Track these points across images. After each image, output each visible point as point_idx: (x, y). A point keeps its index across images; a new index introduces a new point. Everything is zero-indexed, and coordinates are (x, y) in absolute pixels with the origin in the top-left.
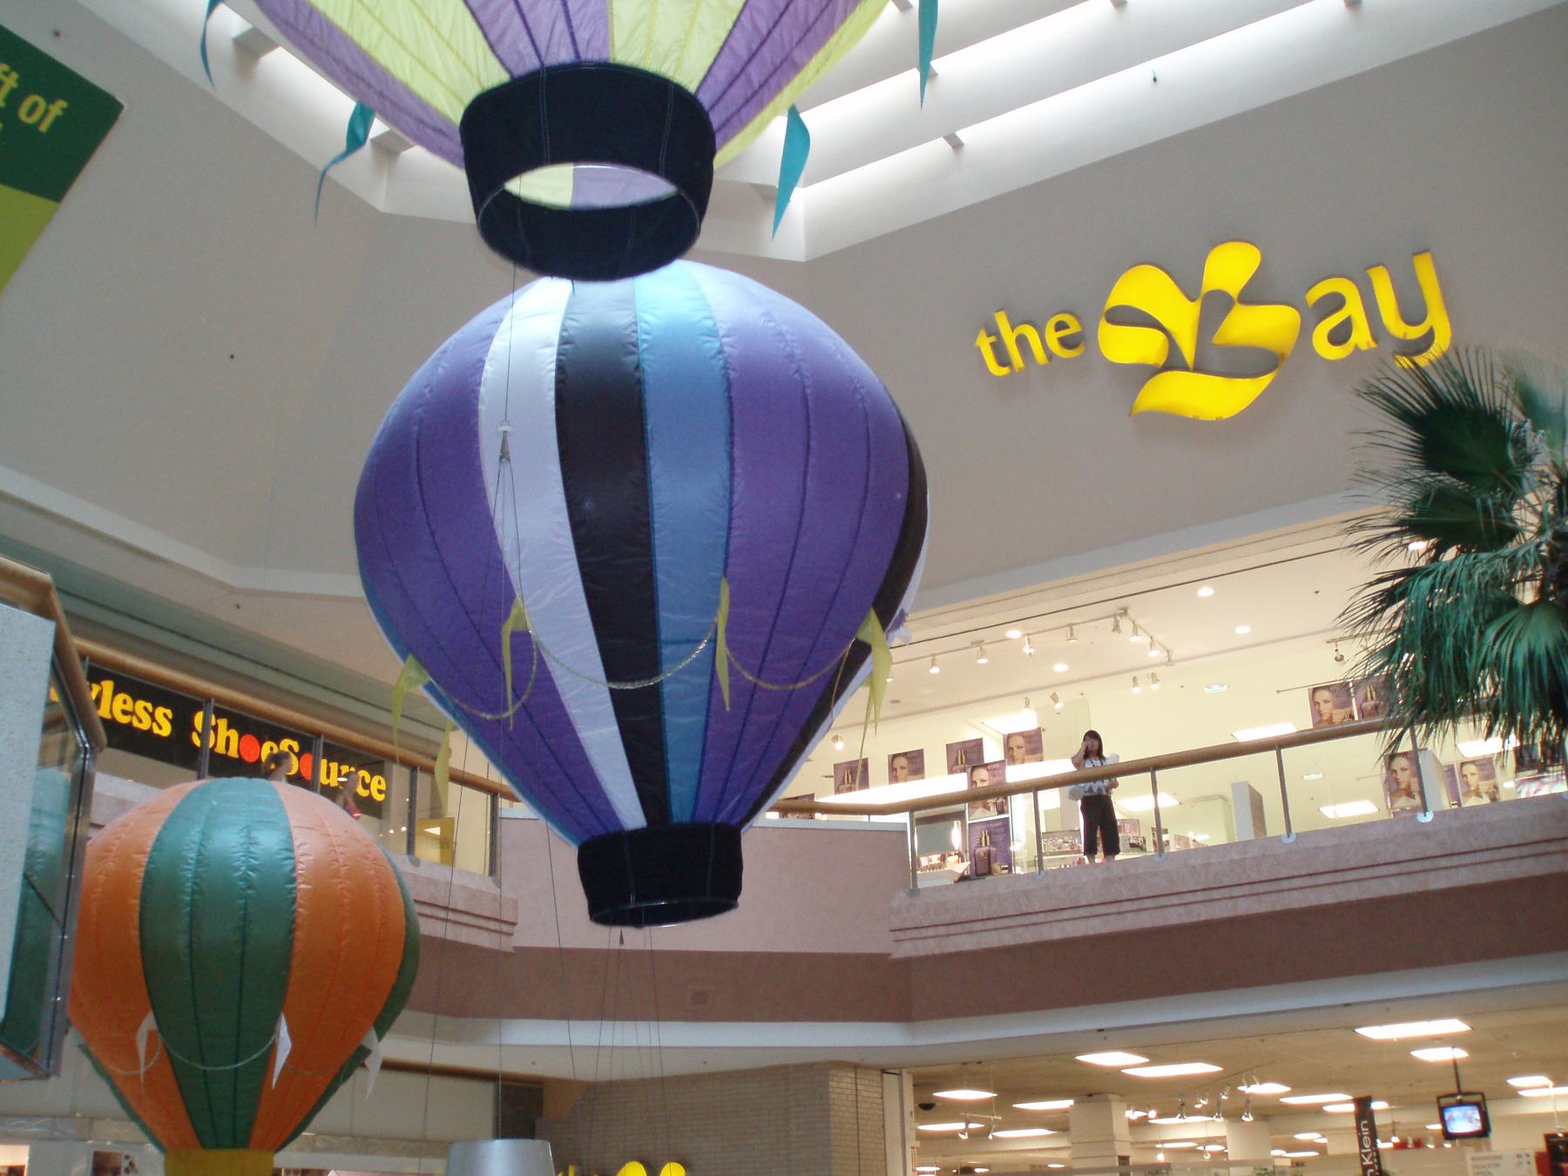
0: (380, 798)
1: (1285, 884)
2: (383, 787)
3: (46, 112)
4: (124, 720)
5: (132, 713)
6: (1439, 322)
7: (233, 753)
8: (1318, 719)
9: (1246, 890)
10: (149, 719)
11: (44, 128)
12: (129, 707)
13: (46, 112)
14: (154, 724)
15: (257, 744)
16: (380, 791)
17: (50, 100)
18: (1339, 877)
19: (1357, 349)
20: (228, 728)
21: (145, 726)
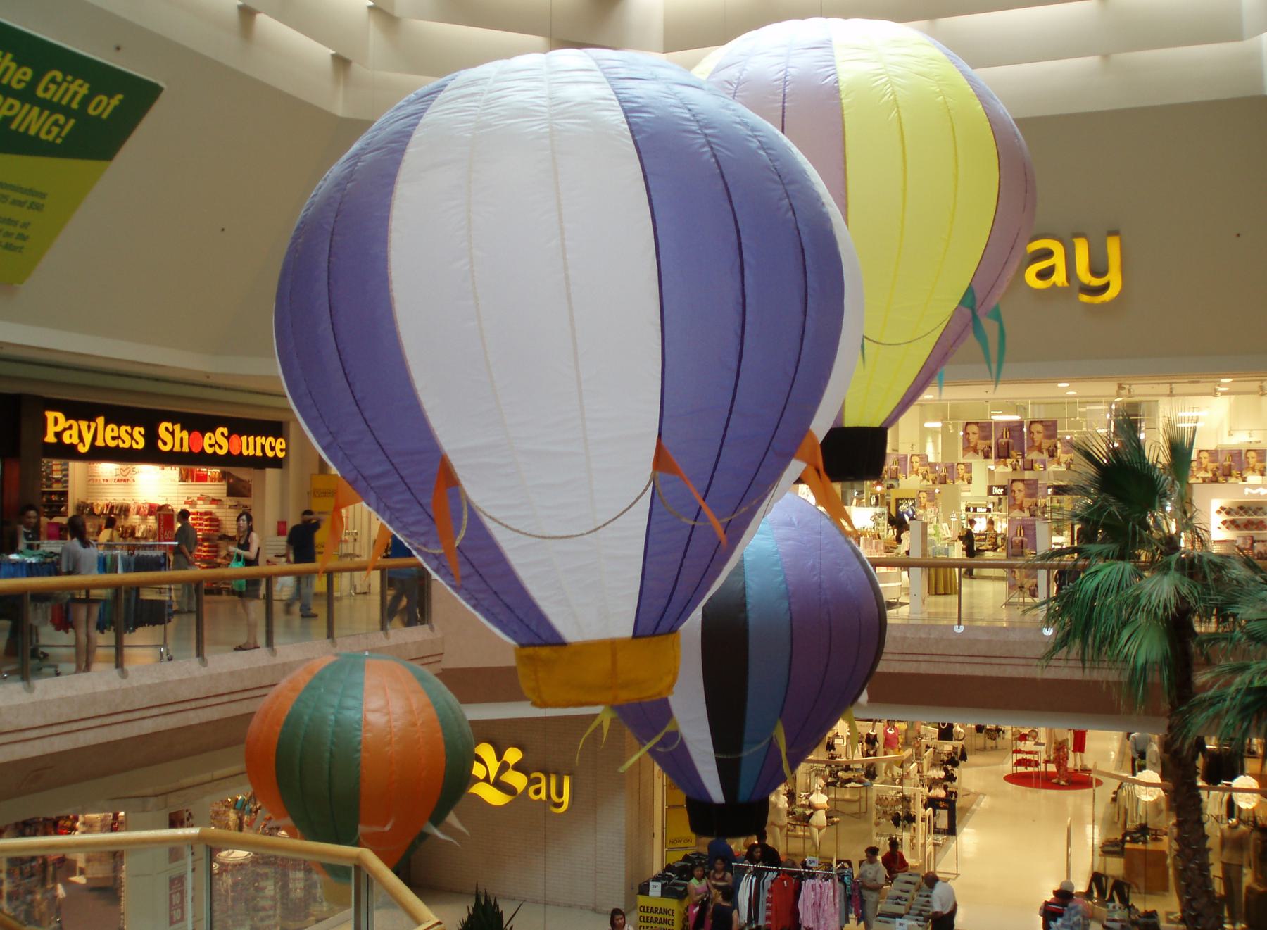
0: (281, 455)
1: (953, 659)
2: (284, 446)
3: (108, 104)
4: (112, 444)
5: (119, 437)
6: (1115, 280)
7: (186, 449)
8: (967, 445)
9: (926, 658)
10: (129, 438)
11: (105, 116)
12: (115, 434)
13: (108, 104)
14: (133, 441)
15: (200, 436)
16: (282, 450)
17: (110, 96)
18: (988, 660)
19: (1054, 284)
20: (181, 430)
21: (127, 445)
